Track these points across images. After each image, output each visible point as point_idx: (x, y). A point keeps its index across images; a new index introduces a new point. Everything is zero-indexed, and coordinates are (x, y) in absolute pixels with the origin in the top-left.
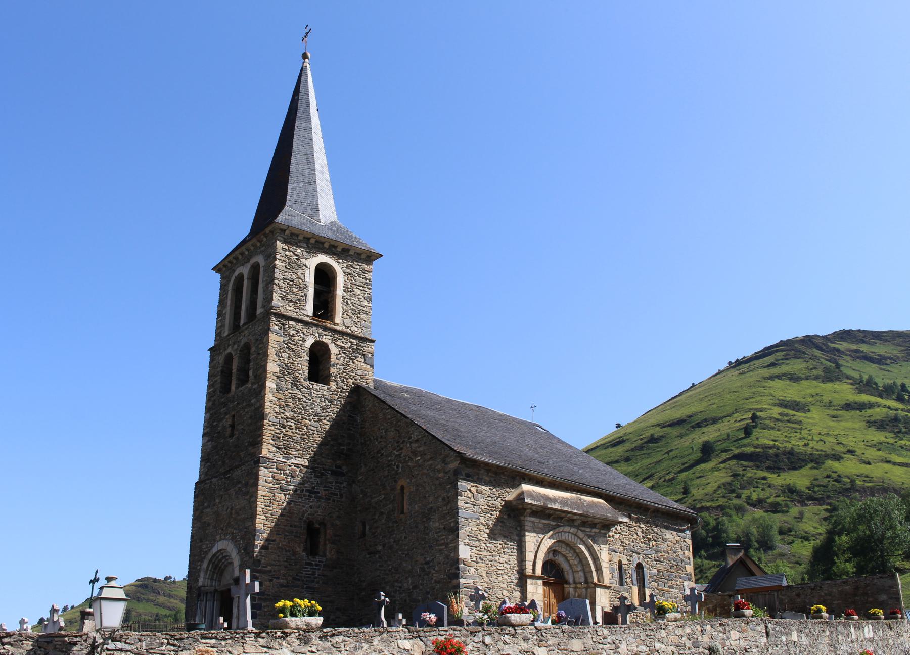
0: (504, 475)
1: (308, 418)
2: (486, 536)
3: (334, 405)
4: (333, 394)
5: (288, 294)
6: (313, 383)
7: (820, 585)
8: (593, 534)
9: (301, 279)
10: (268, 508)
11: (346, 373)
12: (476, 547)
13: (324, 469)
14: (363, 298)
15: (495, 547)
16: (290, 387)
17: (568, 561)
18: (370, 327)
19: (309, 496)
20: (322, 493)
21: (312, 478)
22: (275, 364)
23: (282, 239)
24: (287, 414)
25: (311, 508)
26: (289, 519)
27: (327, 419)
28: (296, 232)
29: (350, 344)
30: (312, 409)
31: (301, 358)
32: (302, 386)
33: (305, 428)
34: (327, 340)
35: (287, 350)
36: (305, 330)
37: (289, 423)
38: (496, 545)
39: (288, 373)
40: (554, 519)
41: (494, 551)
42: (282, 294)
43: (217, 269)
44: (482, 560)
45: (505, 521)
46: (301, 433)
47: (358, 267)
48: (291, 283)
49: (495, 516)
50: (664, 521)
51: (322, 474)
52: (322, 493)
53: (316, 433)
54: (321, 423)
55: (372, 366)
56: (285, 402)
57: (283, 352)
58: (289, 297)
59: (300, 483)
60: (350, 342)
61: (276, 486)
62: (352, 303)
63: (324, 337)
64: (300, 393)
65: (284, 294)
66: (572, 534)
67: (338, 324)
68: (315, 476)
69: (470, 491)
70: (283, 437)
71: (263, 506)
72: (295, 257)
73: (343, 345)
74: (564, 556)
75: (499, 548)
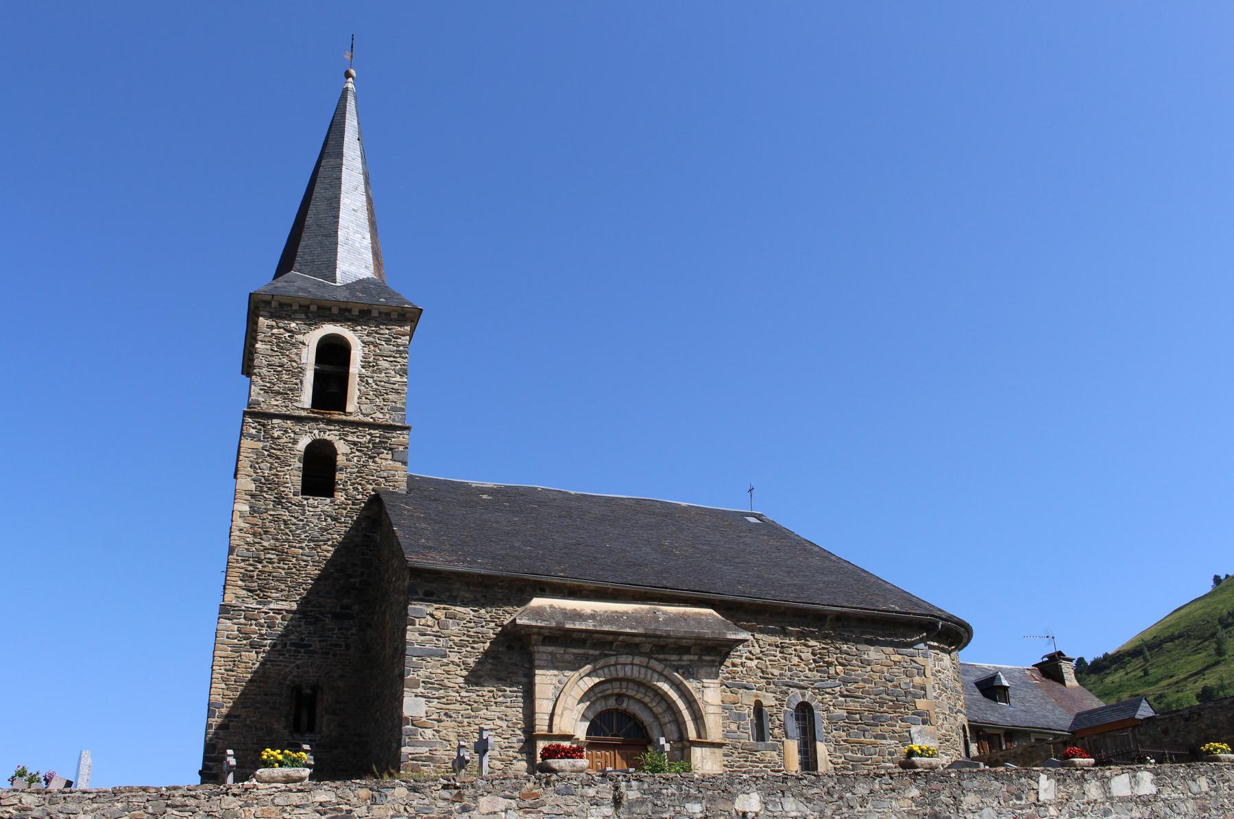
0: (501, 587)
1: (298, 545)
2: (461, 680)
3: (341, 523)
4: (339, 508)
5: (274, 385)
6: (309, 497)
7: (1197, 711)
8: (685, 663)
9: (295, 361)
10: (231, 673)
11: (361, 477)
12: (437, 698)
13: (322, 614)
14: (393, 373)
15: (478, 695)
16: (271, 506)
17: (650, 709)
18: (403, 410)
19: (295, 651)
20: (316, 645)
21: (300, 626)
22: (249, 479)
23: (266, 314)
24: (266, 544)
25: (298, 668)
26: (262, 685)
27: (330, 543)
28: (327, 305)
29: (369, 437)
30: (306, 532)
31: (290, 466)
32: (291, 503)
33: (294, 560)
34: (331, 436)
35: (268, 459)
36: (297, 429)
37: (268, 556)
38: (480, 693)
39: (269, 489)
40: (594, 646)
41: (475, 702)
42: (266, 386)
43: (242, 374)
44: (451, 717)
45: (502, 656)
46: (286, 567)
47: (387, 332)
48: (279, 369)
49: (482, 650)
50: (863, 633)
51: (317, 619)
52: (316, 645)
53: (311, 564)
54: (319, 550)
55: (404, 463)
56: (262, 528)
57: (262, 462)
58: (276, 388)
59: (280, 636)
60: (368, 434)
61: (245, 642)
62: (374, 381)
63: (328, 433)
64: (287, 513)
65: (268, 385)
66: (640, 666)
67: (351, 413)
68: (305, 623)
69: (432, 615)
70: (258, 575)
71: (223, 671)
72: (287, 335)
73: (356, 439)
74: (639, 701)
75: (486, 698)
